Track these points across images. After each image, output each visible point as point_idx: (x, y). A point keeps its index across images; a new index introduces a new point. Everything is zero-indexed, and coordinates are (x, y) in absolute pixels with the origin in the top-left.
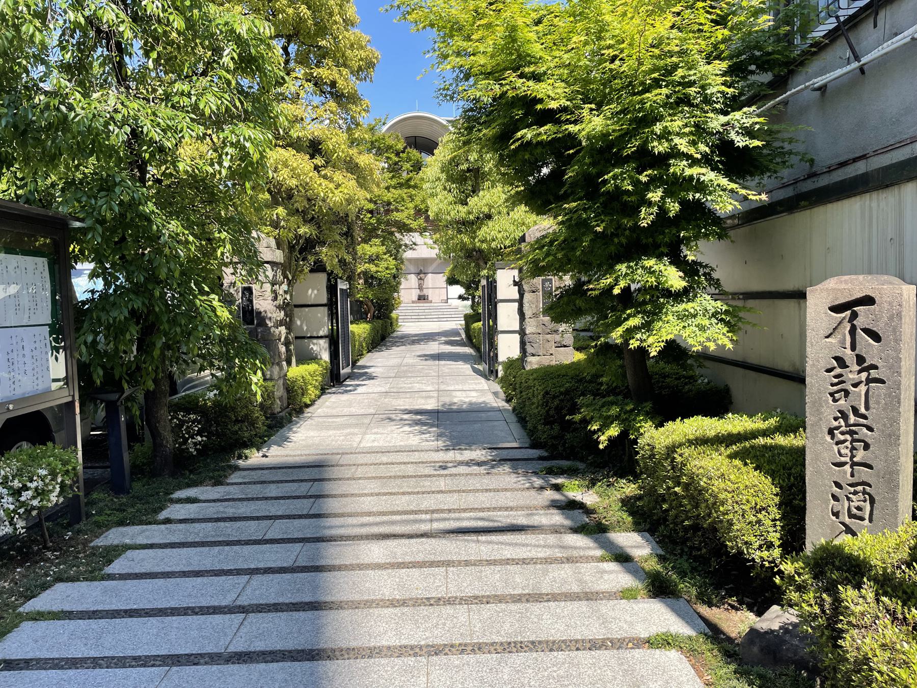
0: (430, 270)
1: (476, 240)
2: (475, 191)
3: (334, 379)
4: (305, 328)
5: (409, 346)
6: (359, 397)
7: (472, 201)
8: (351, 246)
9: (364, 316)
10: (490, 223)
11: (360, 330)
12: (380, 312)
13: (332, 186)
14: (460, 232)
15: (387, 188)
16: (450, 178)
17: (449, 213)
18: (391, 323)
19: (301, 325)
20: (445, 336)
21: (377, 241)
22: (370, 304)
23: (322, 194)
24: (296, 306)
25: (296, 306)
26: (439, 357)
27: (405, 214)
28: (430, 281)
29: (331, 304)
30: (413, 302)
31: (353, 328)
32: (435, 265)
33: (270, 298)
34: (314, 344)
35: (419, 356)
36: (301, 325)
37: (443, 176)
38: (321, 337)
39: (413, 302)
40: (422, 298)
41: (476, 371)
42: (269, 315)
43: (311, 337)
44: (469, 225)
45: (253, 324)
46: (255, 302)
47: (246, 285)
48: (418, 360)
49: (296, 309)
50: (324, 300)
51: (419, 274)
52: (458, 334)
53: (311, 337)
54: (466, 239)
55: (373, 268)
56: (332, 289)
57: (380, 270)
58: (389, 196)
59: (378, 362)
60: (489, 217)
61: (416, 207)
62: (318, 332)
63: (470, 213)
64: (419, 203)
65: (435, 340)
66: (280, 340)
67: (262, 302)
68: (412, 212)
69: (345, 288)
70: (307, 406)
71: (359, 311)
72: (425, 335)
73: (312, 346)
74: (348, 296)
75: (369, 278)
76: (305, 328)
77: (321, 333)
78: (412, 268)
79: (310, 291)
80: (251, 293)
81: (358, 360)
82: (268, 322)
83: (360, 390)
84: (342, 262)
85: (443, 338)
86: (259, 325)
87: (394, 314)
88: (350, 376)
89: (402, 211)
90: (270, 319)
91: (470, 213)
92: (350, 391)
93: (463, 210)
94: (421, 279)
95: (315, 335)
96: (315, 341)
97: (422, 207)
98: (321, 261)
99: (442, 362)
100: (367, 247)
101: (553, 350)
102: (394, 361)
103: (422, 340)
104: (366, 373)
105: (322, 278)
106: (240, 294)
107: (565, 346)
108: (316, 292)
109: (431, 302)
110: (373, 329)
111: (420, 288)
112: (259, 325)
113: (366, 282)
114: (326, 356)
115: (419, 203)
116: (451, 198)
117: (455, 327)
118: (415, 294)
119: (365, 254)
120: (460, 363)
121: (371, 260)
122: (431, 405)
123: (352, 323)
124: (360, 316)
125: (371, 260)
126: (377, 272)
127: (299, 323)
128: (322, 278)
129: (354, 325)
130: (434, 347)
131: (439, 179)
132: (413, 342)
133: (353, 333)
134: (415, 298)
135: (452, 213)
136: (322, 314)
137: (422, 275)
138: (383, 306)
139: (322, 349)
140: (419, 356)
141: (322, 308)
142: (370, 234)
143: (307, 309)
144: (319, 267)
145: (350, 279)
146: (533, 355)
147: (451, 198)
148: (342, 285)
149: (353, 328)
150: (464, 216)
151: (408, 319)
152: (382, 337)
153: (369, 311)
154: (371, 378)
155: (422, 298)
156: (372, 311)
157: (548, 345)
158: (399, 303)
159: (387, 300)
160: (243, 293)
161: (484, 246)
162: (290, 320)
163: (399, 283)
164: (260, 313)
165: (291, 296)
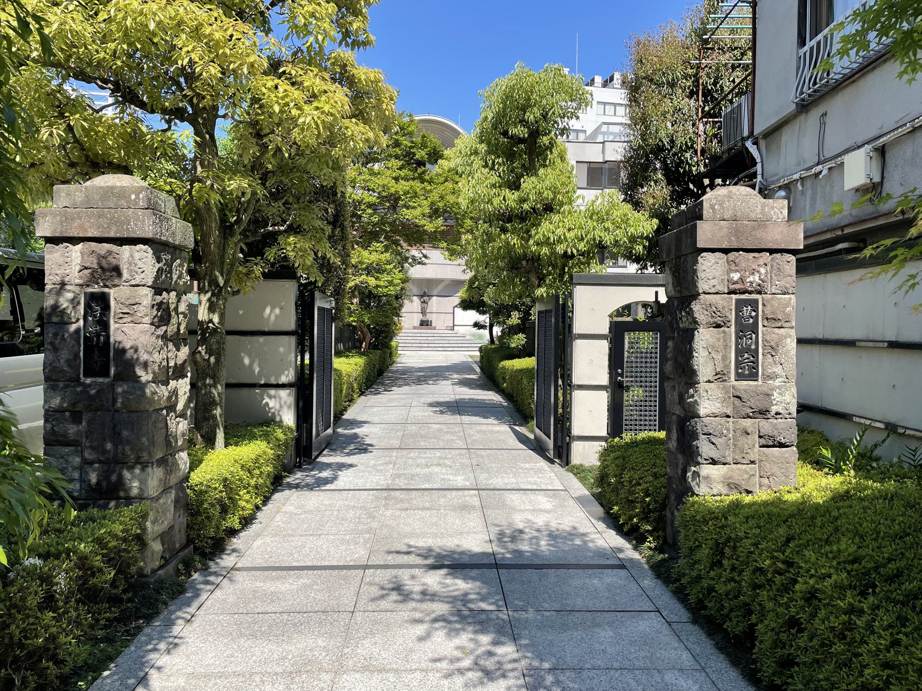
0: (435, 292)
1: (531, 242)
2: (530, 169)
3: (301, 455)
4: (257, 370)
5: (414, 387)
6: (339, 500)
7: (528, 183)
8: (339, 240)
9: (358, 344)
10: (556, 218)
11: (348, 366)
12: (376, 341)
13: (296, 94)
14: (504, 230)
15: (396, 179)
16: (493, 149)
17: (490, 201)
18: (391, 353)
19: (251, 364)
20: (458, 372)
21: (379, 246)
22: (365, 330)
23: (277, 108)
24: (229, 333)
25: (229, 333)
26: (458, 407)
27: (417, 212)
28: (435, 305)
29: (302, 334)
30: (414, 328)
31: (339, 363)
32: (440, 287)
33: (147, 320)
34: (270, 397)
35: (431, 405)
36: (251, 364)
37: (483, 148)
38: (283, 386)
39: (414, 328)
40: (425, 324)
41: (522, 439)
42: (144, 357)
43: (268, 386)
44: (521, 219)
45: (107, 374)
46: (113, 326)
47: (95, 289)
48: (429, 412)
49: (230, 338)
50: (291, 325)
51: (422, 296)
52: (472, 371)
53: (268, 386)
54: (514, 241)
55: (372, 281)
56: (305, 305)
57: (382, 283)
58: (394, 187)
59: (374, 414)
60: (549, 208)
61: (433, 203)
62: (278, 376)
63: (523, 200)
64: (436, 198)
65: (446, 378)
66: (171, 408)
67: (127, 328)
68: (427, 211)
69: (327, 306)
70: (232, 532)
71: (351, 338)
72: (432, 369)
73: (266, 400)
74: (333, 319)
75: (367, 296)
76: (257, 370)
77: (284, 379)
78: (415, 290)
79: (268, 310)
80: (106, 307)
81: (345, 410)
82: (139, 372)
83: (345, 479)
84: (324, 265)
85: (455, 376)
86: (119, 377)
87: (393, 343)
88: (330, 444)
89: (414, 208)
90: (145, 365)
91: (523, 200)
92: (326, 481)
93: (512, 197)
94: (424, 302)
95: (273, 381)
96: (272, 392)
97: (441, 204)
98: (286, 258)
99: (466, 419)
100: (365, 253)
101: (756, 452)
102: (395, 415)
103: (430, 377)
104: (356, 436)
105: (288, 290)
106: (81, 308)
107: (782, 445)
108: (277, 311)
109: (435, 328)
110: (368, 364)
111: (423, 312)
112: (119, 377)
113: (362, 302)
114: (289, 418)
115: (436, 198)
116: (494, 179)
117: (465, 359)
118: (417, 319)
119: (361, 263)
120: (491, 420)
121: (369, 270)
122: (475, 540)
123: (339, 354)
124: (351, 342)
125: (369, 270)
126: (377, 286)
127: (247, 361)
128: (288, 290)
129: (343, 359)
130: (448, 390)
131: (476, 153)
132: (420, 381)
133: (339, 374)
134: (417, 324)
135: (496, 201)
136: (286, 347)
137: (425, 298)
138: (382, 332)
139: (282, 407)
140: (431, 405)
141: (286, 338)
142: (369, 237)
143: (262, 339)
144: (283, 271)
145: (338, 293)
146: (714, 462)
147: (494, 179)
148: (321, 303)
149: (339, 363)
150: (513, 205)
151: (410, 352)
152: (378, 376)
153: (364, 339)
154: (363, 449)
155: (425, 324)
156: (368, 339)
157: (744, 441)
158: (401, 329)
159: (387, 325)
160: (88, 306)
161: (545, 250)
162: (218, 360)
163: (401, 306)
164: (124, 351)
165: (222, 317)
